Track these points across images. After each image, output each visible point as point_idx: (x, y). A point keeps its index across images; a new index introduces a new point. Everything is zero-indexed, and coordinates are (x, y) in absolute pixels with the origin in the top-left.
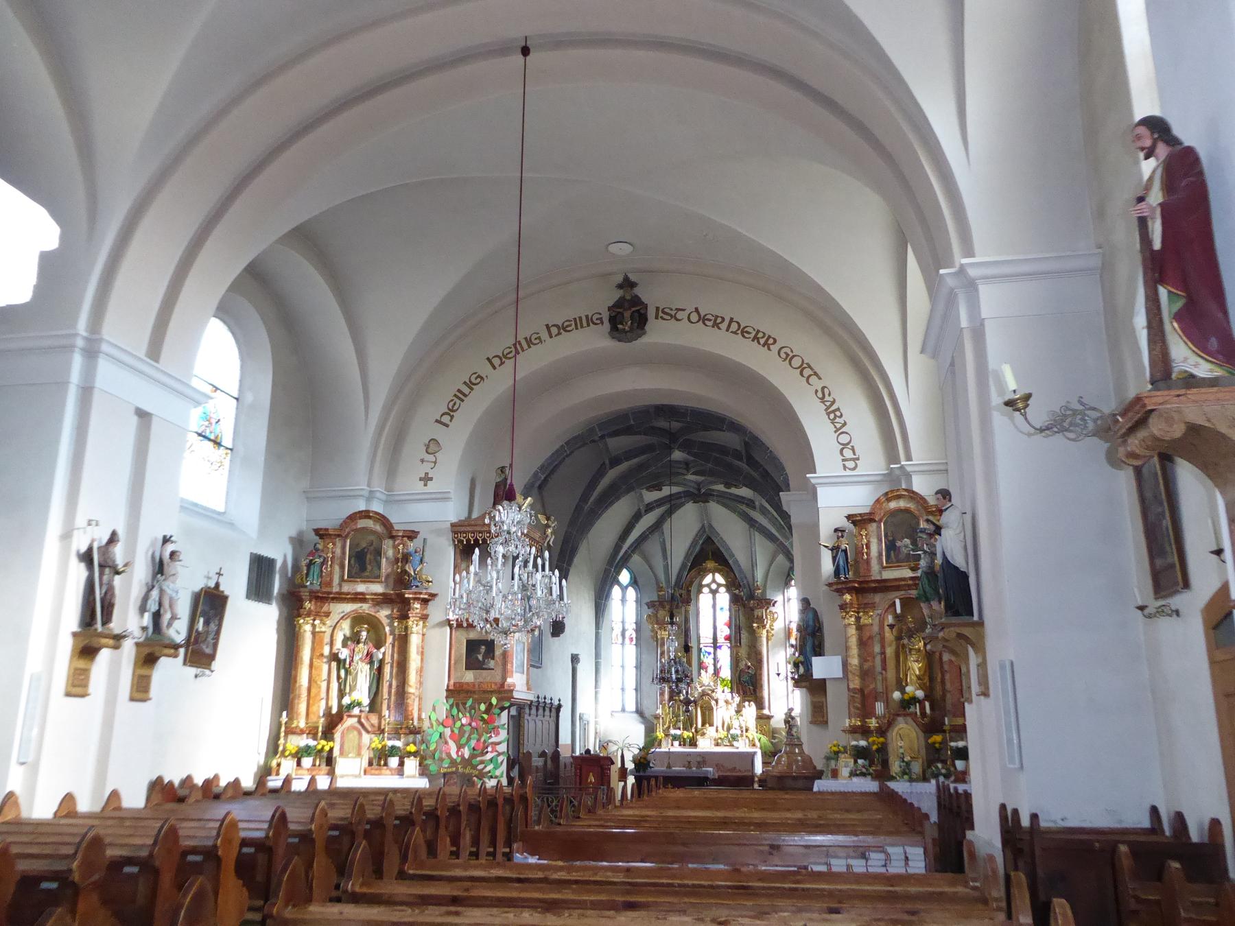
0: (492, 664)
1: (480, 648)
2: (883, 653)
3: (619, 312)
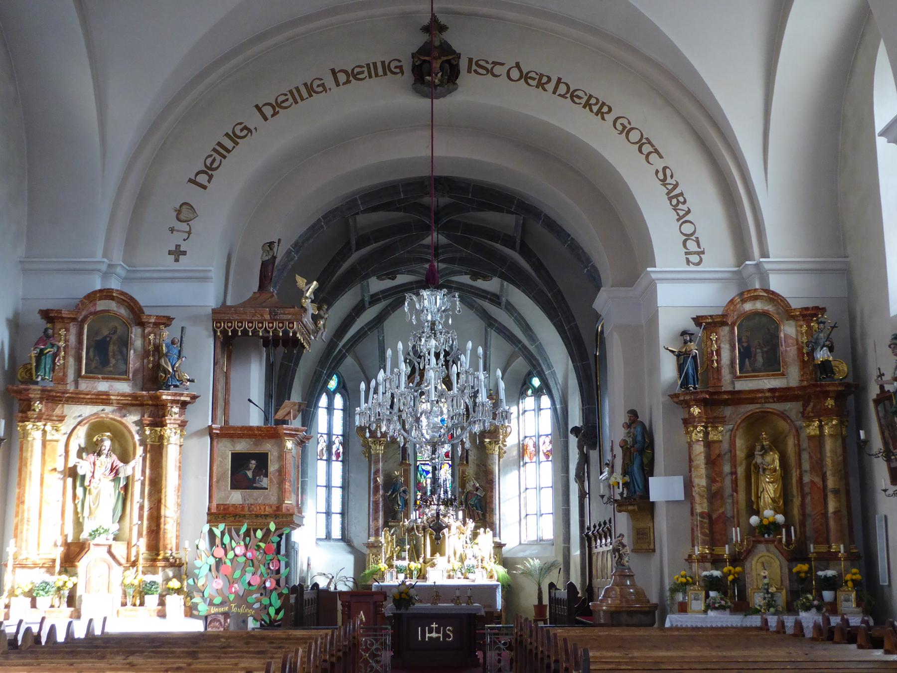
0: (265, 482)
1: (249, 462)
2: (734, 473)
3: (425, 61)
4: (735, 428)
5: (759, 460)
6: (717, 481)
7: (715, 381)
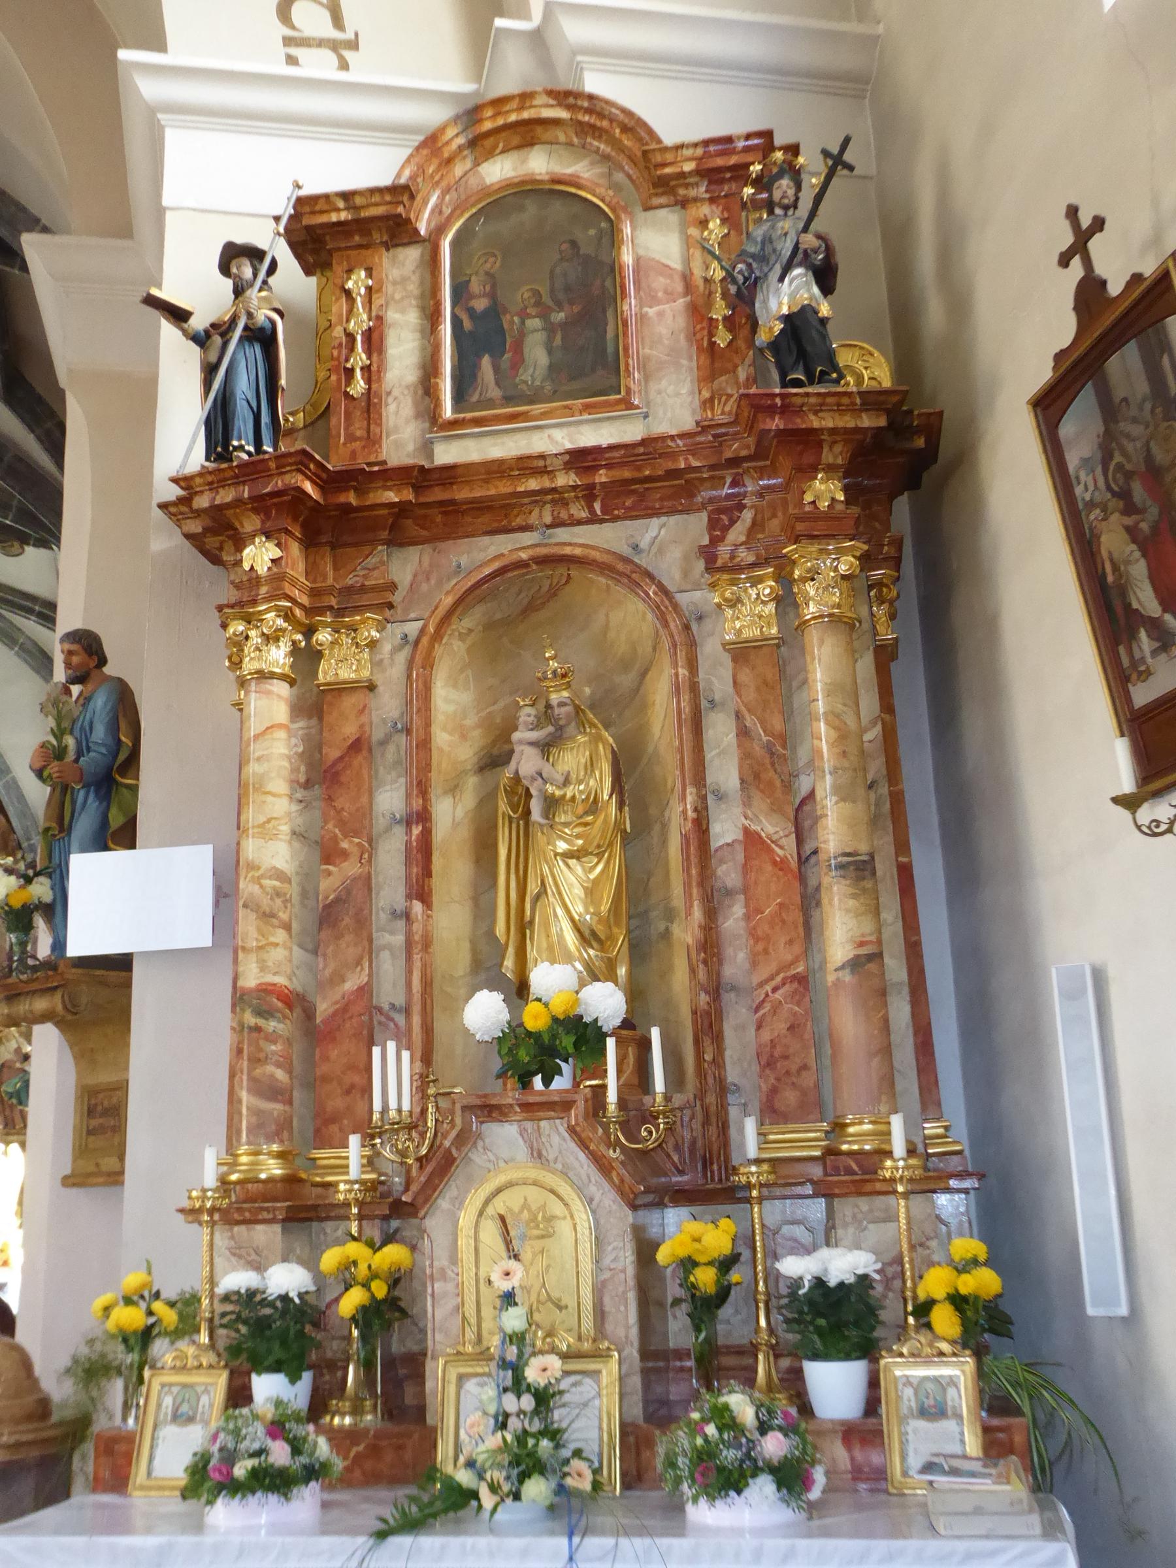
4: (431, 629)
5: (527, 762)
6: (344, 854)
7: (357, 445)
